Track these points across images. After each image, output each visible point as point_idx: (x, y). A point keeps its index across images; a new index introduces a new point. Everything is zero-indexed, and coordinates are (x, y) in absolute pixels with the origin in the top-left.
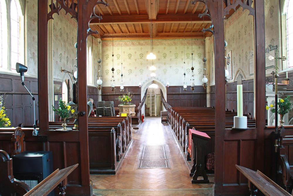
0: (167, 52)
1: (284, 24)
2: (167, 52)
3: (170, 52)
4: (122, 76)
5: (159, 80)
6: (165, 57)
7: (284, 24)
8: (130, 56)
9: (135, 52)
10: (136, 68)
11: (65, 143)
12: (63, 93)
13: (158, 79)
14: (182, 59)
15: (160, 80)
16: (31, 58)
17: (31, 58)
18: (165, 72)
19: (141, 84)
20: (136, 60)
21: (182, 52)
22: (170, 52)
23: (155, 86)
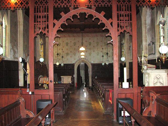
0: (92, 41)
1: (62, 104)
2: (92, 41)
3: (94, 41)
4: (62, 57)
5: (86, 59)
6: (90, 45)
7: (62, 104)
8: (67, 44)
9: (71, 42)
10: (71, 52)
11: (139, 57)
12: (19, 69)
13: (85, 59)
14: (101, 46)
15: (87, 60)
16: (12, 49)
17: (12, 49)
18: (90, 54)
19: (74, 63)
20: (71, 47)
21: (101, 41)
22: (94, 41)
23: (82, 63)
